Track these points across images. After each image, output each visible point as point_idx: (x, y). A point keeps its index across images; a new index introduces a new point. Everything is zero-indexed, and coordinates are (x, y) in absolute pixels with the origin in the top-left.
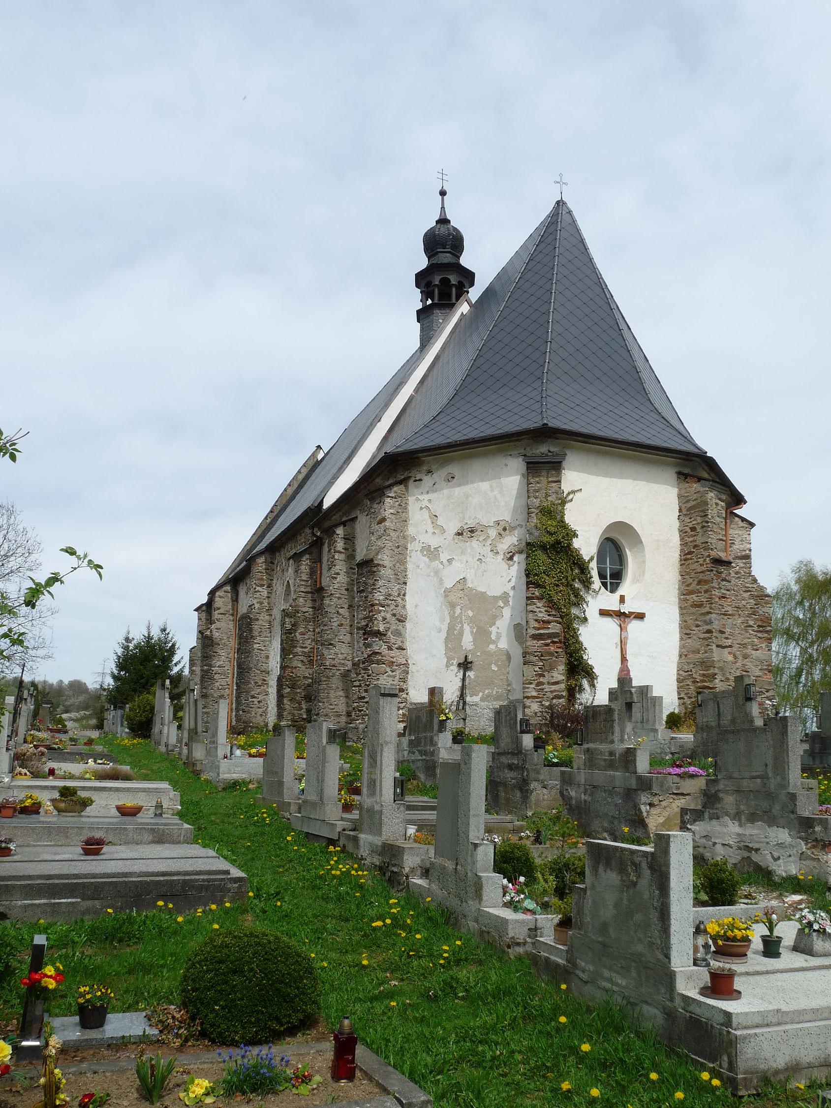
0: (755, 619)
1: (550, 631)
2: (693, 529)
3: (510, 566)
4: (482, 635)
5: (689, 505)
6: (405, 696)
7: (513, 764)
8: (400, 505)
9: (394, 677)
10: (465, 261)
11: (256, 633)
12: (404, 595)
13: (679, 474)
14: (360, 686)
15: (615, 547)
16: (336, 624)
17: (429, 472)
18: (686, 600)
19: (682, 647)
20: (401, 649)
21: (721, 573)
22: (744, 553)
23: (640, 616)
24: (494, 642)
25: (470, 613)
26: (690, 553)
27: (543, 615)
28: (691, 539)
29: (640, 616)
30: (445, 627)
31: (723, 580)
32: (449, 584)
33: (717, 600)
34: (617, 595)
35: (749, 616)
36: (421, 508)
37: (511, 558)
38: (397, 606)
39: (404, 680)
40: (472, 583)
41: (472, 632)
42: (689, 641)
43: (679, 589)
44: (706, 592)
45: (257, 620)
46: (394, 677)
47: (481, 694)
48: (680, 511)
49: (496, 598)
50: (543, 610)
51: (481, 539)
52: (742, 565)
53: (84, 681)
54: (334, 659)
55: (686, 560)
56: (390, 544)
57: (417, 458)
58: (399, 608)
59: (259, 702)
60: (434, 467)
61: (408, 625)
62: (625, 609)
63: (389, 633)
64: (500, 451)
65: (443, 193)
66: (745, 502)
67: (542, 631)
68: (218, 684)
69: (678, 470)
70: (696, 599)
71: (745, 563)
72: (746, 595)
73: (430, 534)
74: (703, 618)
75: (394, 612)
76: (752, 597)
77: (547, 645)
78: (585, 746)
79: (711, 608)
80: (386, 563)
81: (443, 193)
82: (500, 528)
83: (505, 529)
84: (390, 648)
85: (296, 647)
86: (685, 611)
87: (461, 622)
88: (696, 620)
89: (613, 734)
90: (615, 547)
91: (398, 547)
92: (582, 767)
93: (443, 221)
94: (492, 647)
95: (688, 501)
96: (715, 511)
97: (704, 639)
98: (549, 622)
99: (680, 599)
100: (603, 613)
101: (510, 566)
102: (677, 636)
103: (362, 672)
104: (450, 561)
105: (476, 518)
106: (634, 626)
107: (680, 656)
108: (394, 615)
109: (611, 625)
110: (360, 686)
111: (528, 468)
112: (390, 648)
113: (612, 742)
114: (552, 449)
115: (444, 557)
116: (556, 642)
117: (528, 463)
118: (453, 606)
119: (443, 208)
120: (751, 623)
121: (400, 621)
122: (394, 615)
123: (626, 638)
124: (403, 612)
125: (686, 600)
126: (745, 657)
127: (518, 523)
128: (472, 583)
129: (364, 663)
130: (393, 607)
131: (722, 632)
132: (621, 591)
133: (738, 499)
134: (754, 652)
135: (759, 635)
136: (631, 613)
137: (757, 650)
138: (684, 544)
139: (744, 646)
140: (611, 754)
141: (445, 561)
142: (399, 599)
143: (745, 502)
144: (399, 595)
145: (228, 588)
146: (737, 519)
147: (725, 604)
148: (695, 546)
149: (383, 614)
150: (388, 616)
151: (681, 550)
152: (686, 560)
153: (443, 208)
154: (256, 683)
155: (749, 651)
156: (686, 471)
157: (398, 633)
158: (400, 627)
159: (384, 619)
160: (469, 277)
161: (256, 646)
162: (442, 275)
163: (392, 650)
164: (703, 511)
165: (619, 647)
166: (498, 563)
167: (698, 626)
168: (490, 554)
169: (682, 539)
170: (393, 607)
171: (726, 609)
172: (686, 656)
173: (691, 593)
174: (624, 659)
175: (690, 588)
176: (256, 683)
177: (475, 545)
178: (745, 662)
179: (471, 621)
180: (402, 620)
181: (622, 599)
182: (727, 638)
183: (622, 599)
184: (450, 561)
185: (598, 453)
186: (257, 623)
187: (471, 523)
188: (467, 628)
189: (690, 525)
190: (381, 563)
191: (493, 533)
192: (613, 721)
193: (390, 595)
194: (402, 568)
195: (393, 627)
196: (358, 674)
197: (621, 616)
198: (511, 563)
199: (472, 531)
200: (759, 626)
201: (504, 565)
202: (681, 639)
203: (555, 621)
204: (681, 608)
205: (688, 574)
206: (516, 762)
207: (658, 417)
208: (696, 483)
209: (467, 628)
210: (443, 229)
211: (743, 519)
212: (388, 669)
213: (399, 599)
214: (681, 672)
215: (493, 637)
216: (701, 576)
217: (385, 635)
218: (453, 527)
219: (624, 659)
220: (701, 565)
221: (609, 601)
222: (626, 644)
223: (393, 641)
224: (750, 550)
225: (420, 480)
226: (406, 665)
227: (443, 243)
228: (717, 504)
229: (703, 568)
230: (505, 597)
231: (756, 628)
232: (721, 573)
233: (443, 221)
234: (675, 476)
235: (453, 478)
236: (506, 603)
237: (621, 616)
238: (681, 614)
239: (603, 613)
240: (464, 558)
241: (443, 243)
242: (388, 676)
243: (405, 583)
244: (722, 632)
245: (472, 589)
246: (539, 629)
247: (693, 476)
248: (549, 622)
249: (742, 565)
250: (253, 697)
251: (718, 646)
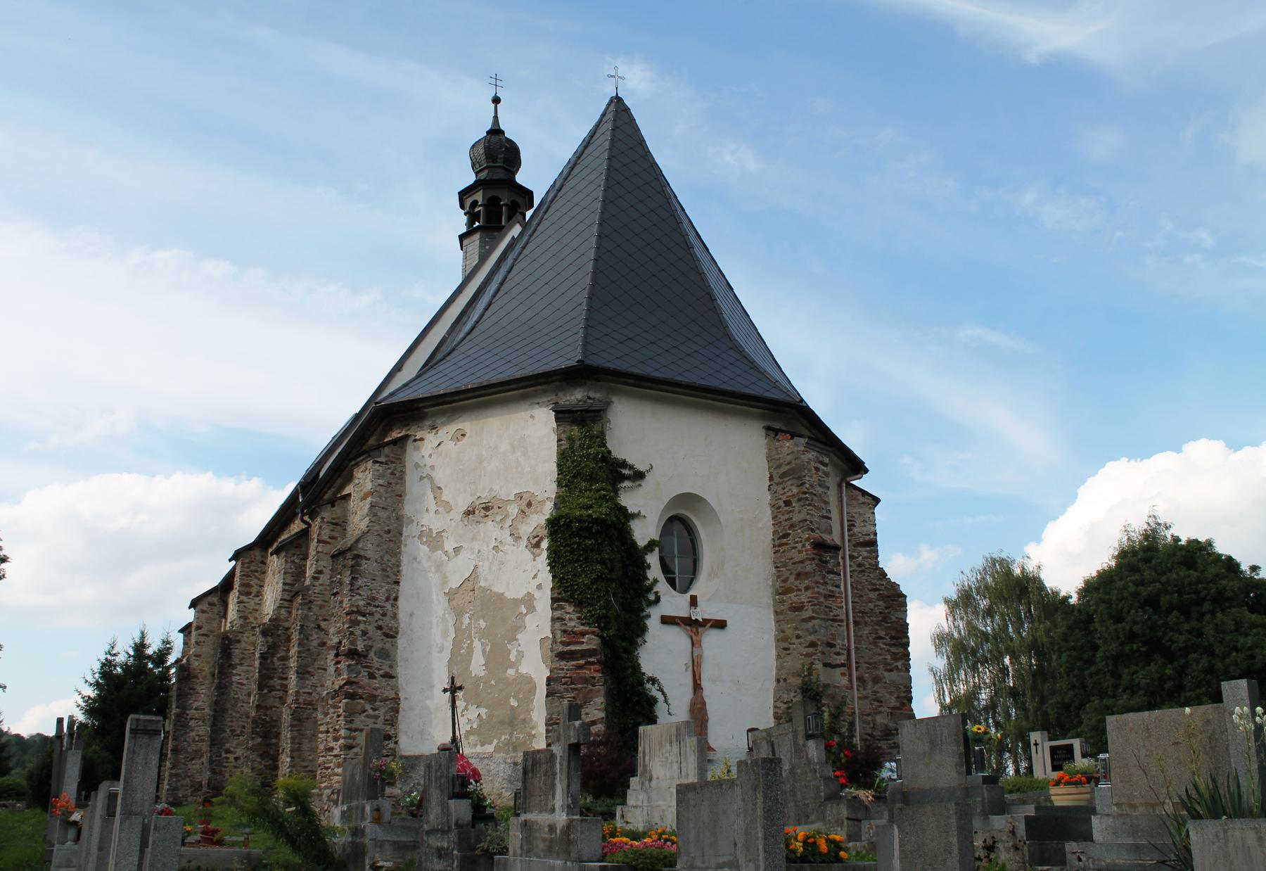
0: (887, 628)
1: (584, 647)
2: (788, 503)
3: (535, 556)
4: (498, 658)
5: (781, 471)
6: (392, 746)
7: (442, 848)
8: (392, 474)
9: (377, 717)
10: (521, 178)
11: (236, 661)
12: (396, 599)
13: (768, 428)
14: (328, 732)
15: (681, 525)
16: (315, 643)
17: (434, 428)
18: (782, 602)
19: (779, 668)
20: (389, 676)
21: (826, 562)
22: (867, 538)
23: (720, 625)
24: (513, 665)
25: (482, 624)
26: (786, 536)
27: (574, 624)
28: (787, 517)
29: (720, 625)
30: (449, 645)
31: (829, 572)
32: (455, 583)
33: (822, 599)
34: (687, 596)
35: (878, 623)
36: (422, 478)
37: (537, 545)
38: (384, 615)
39: (392, 722)
40: (486, 580)
41: (484, 651)
42: (788, 658)
43: (773, 585)
44: (807, 588)
45: (239, 641)
46: (377, 717)
47: (495, 742)
48: (771, 478)
49: (517, 602)
50: (574, 616)
51: (498, 518)
52: (866, 554)
53: (34, 733)
54: (310, 694)
55: (780, 545)
56: (377, 528)
57: (418, 409)
58: (387, 618)
59: (236, 759)
60: (439, 421)
61: (401, 642)
62: (698, 615)
63: (372, 654)
64: (524, 398)
65: (496, 100)
66: (866, 471)
67: (573, 648)
68: (193, 734)
69: (765, 424)
70: (795, 599)
71: (869, 552)
72: (873, 595)
73: (432, 513)
74: (805, 625)
75: (380, 623)
76: (881, 597)
77: (580, 667)
78: (523, 817)
79: (813, 611)
80: (369, 554)
81: (496, 100)
82: (524, 502)
83: (529, 504)
84: (372, 676)
85: (272, 678)
86: (781, 617)
87: (470, 637)
88: (796, 628)
89: (554, 797)
90: (681, 525)
91: (389, 532)
92: (519, 851)
93: (496, 131)
94: (511, 672)
95: (779, 467)
96: (815, 478)
97: (806, 655)
98: (583, 634)
99: (774, 600)
100: (667, 620)
101: (535, 556)
102: (773, 653)
103: (332, 710)
104: (457, 550)
105: (491, 489)
106: (711, 638)
107: (778, 681)
108: (380, 628)
109: (678, 638)
110: (328, 732)
111: (557, 419)
112: (372, 676)
113: (553, 810)
114: (592, 395)
115: (449, 545)
116: (592, 663)
117: (557, 412)
118: (458, 614)
119: (496, 117)
120: (882, 634)
121: (387, 635)
122: (380, 628)
123: (700, 656)
124: (393, 623)
125: (782, 602)
126: (876, 680)
127: (546, 495)
128: (486, 580)
129: (333, 698)
130: (378, 616)
131: (831, 645)
132: (692, 592)
133: (858, 467)
134: (887, 674)
135: (893, 650)
136: (706, 621)
137: (891, 670)
138: (777, 523)
139: (874, 665)
140: (552, 828)
141: (451, 550)
142: (388, 605)
143: (866, 471)
144: (388, 599)
145: (215, 599)
146: (856, 492)
147: (834, 606)
148: (792, 526)
149: (362, 626)
150: (371, 629)
151: (775, 532)
152: (780, 545)
153: (496, 117)
154: (233, 731)
155: (881, 672)
156: (777, 426)
157: (385, 655)
158: (388, 646)
159: (365, 633)
160: (529, 194)
161: (235, 679)
162: (495, 193)
163: (374, 678)
164: (798, 478)
165: (690, 669)
166: (520, 553)
167: (798, 637)
168: (510, 540)
169: (774, 518)
170: (378, 616)
171: (835, 612)
172: (785, 680)
173: (787, 591)
174: (697, 687)
175: (788, 585)
176: (233, 731)
177: (490, 530)
178: (877, 687)
179: (483, 634)
180: (391, 635)
181: (694, 601)
182: (838, 654)
183: (694, 601)
184: (457, 550)
185: (656, 400)
186: (238, 646)
187: (485, 496)
188: (477, 645)
189: (784, 498)
190: (362, 553)
191: (513, 510)
192: (554, 774)
193: (374, 599)
194: (393, 561)
195: (379, 645)
196: (326, 714)
197: (693, 625)
198: (537, 551)
199: (487, 509)
200: (892, 638)
201: (528, 555)
202: (779, 656)
203: (593, 633)
204: (776, 613)
205: (785, 565)
206: (445, 845)
207: (738, 356)
208: (788, 440)
209: (477, 645)
210: (495, 138)
211: (864, 493)
212: (368, 707)
213: (388, 605)
214: (779, 704)
215: (513, 657)
216: (799, 568)
217: (365, 657)
218: (463, 503)
219: (697, 687)
220: (800, 552)
221: (672, 602)
222: (699, 665)
223: (377, 665)
224: (875, 534)
225: (422, 439)
226: (396, 700)
227: (498, 155)
228: (817, 469)
229: (803, 556)
230: (529, 600)
231: (888, 640)
232: (826, 562)
233: (496, 131)
234: (763, 432)
235: (463, 435)
236: (531, 609)
237: (693, 625)
238: (777, 621)
239: (667, 620)
240: (476, 546)
241: (498, 155)
242: (368, 716)
243: (397, 583)
244: (831, 645)
245: (485, 590)
246: (568, 644)
247: (786, 432)
248: (583, 634)
249: (866, 554)
250: (228, 751)
251: (826, 665)
